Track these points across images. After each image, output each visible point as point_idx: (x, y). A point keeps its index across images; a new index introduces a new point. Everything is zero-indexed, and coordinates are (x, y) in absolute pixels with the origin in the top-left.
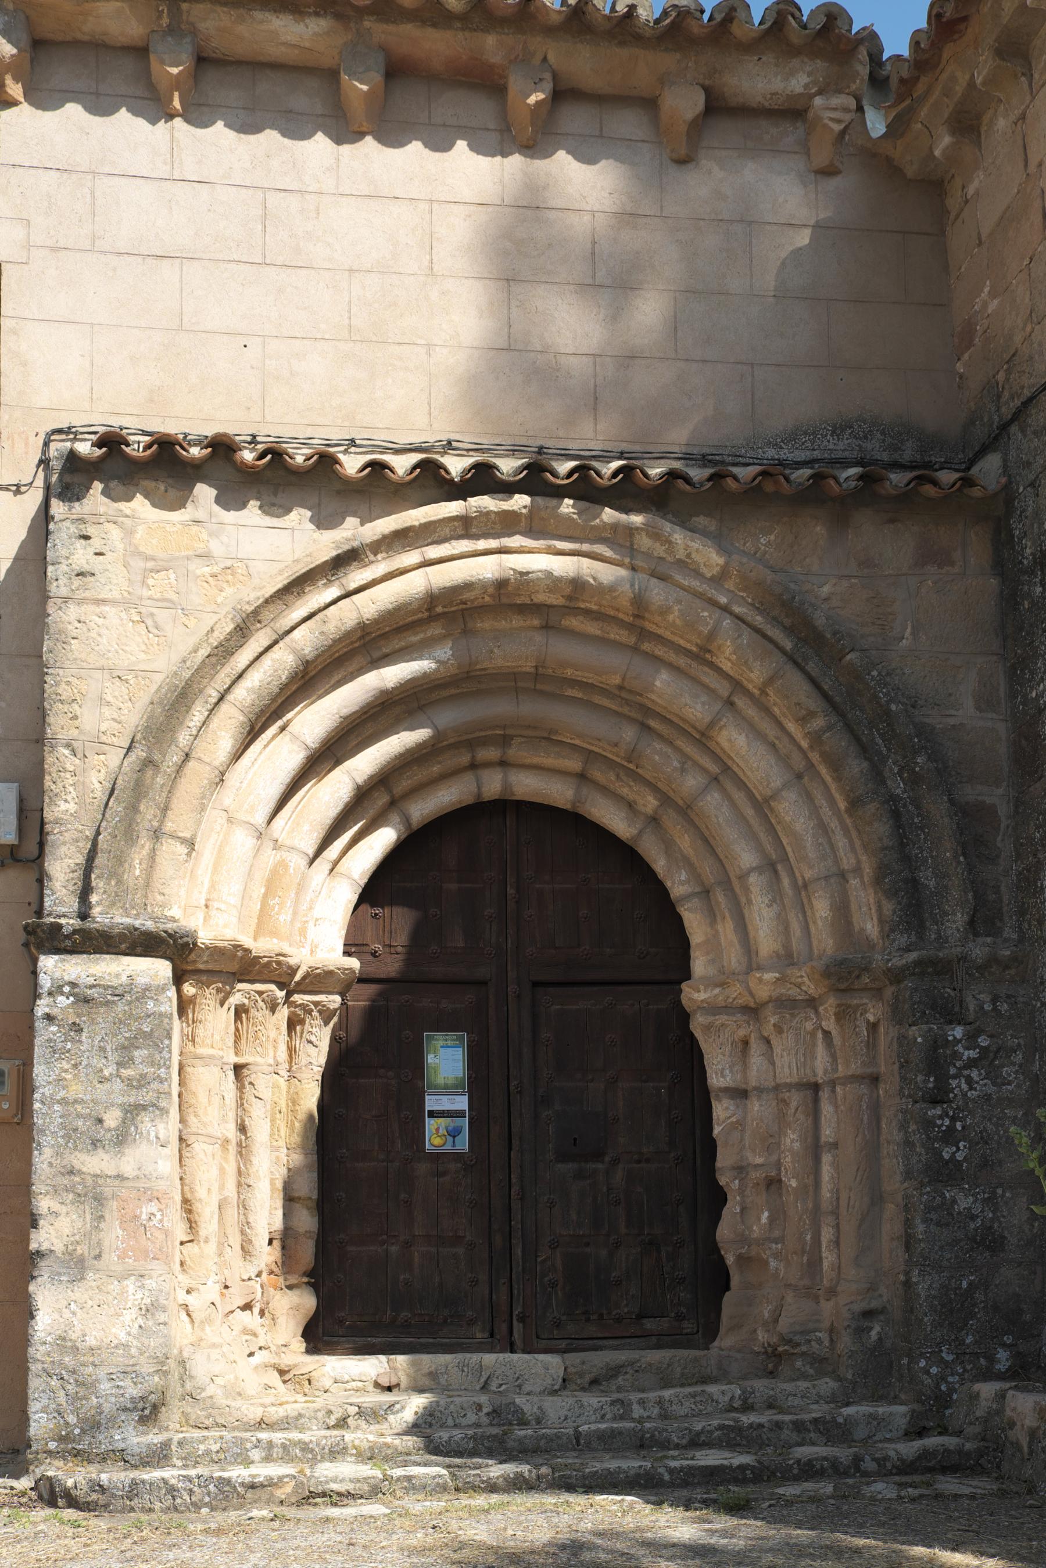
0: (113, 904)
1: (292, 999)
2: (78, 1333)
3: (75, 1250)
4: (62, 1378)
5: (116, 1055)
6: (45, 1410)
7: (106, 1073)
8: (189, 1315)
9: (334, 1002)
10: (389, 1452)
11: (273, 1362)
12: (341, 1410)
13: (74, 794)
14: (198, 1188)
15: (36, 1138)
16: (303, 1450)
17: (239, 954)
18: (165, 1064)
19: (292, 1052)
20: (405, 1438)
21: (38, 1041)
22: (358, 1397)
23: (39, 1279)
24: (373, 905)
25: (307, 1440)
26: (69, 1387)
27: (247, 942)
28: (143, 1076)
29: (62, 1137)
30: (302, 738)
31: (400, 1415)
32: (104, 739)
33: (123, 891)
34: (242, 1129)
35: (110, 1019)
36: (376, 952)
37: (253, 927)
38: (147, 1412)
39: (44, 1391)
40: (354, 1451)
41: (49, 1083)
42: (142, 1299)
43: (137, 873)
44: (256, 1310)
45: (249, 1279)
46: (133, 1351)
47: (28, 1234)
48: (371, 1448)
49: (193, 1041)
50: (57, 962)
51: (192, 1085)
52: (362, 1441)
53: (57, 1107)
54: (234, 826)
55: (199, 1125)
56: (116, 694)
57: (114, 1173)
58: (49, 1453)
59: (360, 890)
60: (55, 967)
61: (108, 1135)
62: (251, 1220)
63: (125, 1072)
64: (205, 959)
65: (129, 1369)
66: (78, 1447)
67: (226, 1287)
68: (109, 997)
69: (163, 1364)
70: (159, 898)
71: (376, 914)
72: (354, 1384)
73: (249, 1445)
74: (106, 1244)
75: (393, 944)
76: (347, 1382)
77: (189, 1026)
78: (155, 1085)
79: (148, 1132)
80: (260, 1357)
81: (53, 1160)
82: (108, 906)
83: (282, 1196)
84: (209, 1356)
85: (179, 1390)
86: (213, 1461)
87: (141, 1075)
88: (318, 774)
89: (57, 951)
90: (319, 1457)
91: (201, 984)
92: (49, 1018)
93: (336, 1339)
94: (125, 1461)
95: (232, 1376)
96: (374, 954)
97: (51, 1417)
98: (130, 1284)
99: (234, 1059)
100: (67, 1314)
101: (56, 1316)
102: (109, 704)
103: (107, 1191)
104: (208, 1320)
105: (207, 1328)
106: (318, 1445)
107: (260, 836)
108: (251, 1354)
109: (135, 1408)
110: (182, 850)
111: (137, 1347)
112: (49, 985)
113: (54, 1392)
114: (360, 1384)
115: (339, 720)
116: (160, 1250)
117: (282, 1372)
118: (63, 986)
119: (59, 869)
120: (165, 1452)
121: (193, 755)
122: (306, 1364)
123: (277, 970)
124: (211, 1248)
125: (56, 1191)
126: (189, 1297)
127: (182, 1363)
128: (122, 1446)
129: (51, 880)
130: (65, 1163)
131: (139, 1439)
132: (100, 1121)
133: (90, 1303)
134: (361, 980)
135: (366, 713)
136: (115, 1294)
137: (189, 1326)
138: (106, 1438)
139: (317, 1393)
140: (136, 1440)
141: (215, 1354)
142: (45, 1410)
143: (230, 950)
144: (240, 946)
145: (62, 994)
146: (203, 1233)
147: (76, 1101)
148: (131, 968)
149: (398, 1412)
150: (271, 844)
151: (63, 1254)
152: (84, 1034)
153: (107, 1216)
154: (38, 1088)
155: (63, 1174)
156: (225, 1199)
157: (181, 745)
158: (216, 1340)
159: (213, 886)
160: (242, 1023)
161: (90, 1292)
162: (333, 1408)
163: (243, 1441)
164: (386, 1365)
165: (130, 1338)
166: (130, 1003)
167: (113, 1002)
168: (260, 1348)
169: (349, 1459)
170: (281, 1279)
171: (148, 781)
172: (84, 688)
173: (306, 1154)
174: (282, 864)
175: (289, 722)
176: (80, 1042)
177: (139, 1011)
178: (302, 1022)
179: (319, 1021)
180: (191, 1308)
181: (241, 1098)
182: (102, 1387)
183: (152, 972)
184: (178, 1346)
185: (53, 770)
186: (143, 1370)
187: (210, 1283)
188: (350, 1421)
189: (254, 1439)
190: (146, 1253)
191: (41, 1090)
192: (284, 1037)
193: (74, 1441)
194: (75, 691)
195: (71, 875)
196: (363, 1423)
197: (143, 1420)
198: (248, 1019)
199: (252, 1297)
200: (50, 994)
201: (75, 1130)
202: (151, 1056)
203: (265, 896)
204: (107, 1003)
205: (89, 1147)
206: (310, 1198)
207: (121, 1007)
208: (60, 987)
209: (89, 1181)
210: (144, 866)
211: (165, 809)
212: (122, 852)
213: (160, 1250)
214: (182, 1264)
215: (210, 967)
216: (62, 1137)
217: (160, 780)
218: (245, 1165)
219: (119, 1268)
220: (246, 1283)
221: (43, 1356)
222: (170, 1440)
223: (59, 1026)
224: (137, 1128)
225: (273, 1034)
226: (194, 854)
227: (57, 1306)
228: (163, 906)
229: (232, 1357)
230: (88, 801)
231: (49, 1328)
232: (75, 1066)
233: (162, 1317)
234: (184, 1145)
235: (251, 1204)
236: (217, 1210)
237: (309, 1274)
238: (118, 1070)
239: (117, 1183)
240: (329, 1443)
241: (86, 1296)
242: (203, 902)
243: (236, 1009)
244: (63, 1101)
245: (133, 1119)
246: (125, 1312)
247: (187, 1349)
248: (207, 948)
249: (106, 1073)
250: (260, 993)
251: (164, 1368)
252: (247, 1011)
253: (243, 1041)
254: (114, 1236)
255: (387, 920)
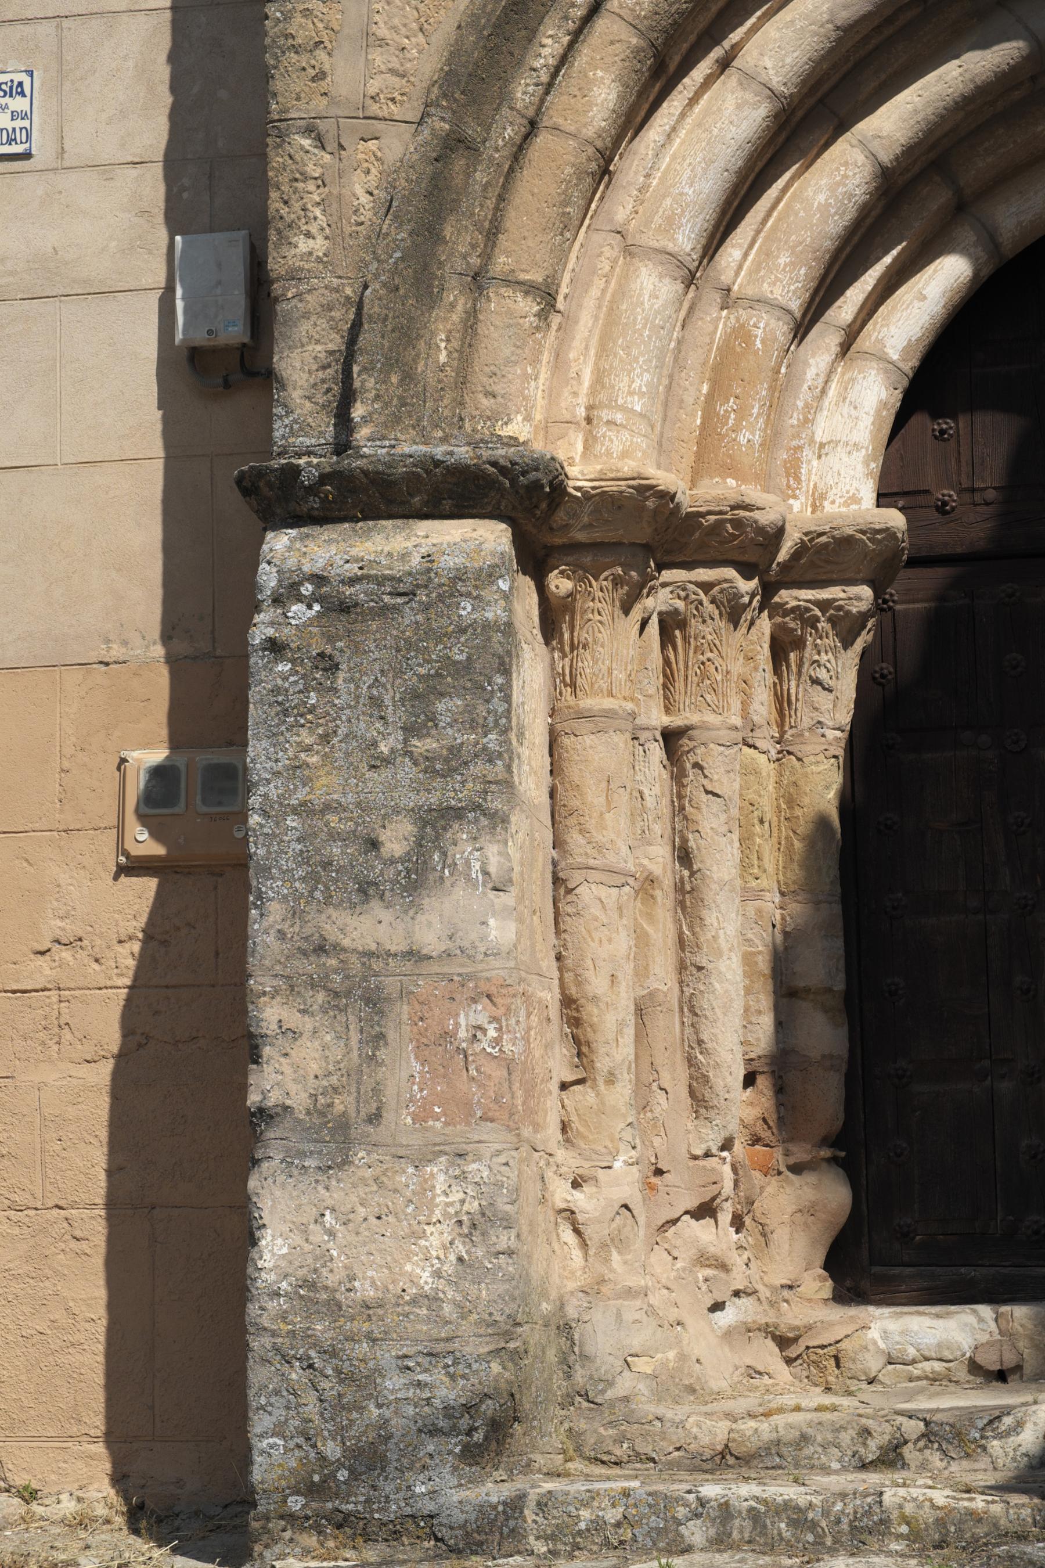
0: (396, 420)
1: (777, 599)
2: (340, 1274)
3: (331, 1105)
4: (311, 1366)
5: (401, 712)
6: (278, 1430)
7: (384, 748)
8: (577, 1231)
9: (859, 598)
10: (980, 1531)
11: (762, 1320)
12: (887, 1428)
13: (322, 220)
14: (590, 974)
15: (254, 883)
16: (793, 1523)
17: (650, 504)
18: (496, 722)
19: (782, 703)
20: (1016, 1499)
21: (253, 694)
22: (931, 1396)
23: (265, 1165)
24: (936, 415)
25: (802, 1501)
26: (325, 1384)
27: (665, 478)
28: (454, 750)
29: (303, 879)
30: (763, 78)
31: (1013, 1440)
32: (374, 109)
33: (416, 395)
34: (684, 856)
35: (390, 641)
36: (945, 504)
37: (689, 459)
38: (478, 1437)
39: (277, 1392)
40: (904, 1529)
41: (277, 774)
42: (463, 1202)
43: (443, 357)
44: (725, 1217)
45: (708, 1155)
46: (447, 1309)
47: (245, 1075)
48: (940, 1523)
49: (573, 685)
50: (292, 540)
51: (573, 772)
52: (920, 1507)
53: (291, 821)
54: (636, 261)
55: (589, 849)
56: (396, 21)
57: (403, 947)
58: (290, 1518)
59: (906, 383)
60: (289, 549)
61: (390, 873)
62: (705, 1037)
63: (421, 745)
64: (586, 519)
65: (439, 1347)
66: (343, 1507)
67: (659, 1172)
68: (387, 599)
69: (508, 1336)
70: (486, 402)
71: (942, 432)
72: (927, 1366)
73: (681, 1512)
74: (389, 1096)
75: (978, 485)
76: (914, 1362)
77: (564, 656)
78: (479, 768)
79: (468, 863)
80: (726, 1318)
81: (285, 927)
82: (385, 425)
83: (770, 987)
84: (619, 1315)
85: (559, 1385)
86: (607, 1544)
87: (451, 749)
88: (803, 154)
89: (297, 520)
90: (829, 1541)
91: (582, 572)
92: (275, 647)
93: (897, 1270)
94: (437, 1539)
95: (671, 1355)
96: (942, 509)
97: (291, 1444)
98: (438, 1173)
99: (658, 718)
100: (318, 1236)
101: (297, 1239)
102: (382, 42)
103: (391, 984)
104: (618, 1241)
105: (615, 1256)
106: (826, 1513)
107: (690, 280)
108: (717, 1307)
109: (454, 1427)
110: (528, 306)
111: (454, 1301)
112: (273, 584)
113: (295, 1395)
114: (938, 1366)
115: (833, 36)
116: (496, 1101)
117: (783, 1342)
118: (300, 583)
119: (298, 365)
120: (512, 1523)
121: (546, 121)
122: (828, 1325)
123: (734, 537)
124: (622, 1093)
125: (292, 987)
126: (577, 1195)
127: (566, 1329)
128: (429, 1507)
129: (283, 387)
130: (308, 930)
131: (463, 1494)
132: (374, 844)
133: (362, 1211)
134: (913, 562)
135: (889, 20)
136: (409, 1194)
137: (577, 1254)
138: (398, 1490)
139: (854, 1384)
140: (456, 1496)
141: (632, 1309)
142: (278, 1430)
143: (631, 497)
144: (651, 487)
145: (299, 598)
146: (602, 1064)
147: (327, 808)
148: (430, 541)
149: (1007, 1434)
150: (717, 297)
151: (308, 1113)
152: (341, 675)
153: (391, 1035)
154: (256, 785)
155: (304, 953)
156: (652, 995)
157: (519, 105)
158: (637, 1281)
159: (599, 380)
160: (675, 649)
161: (361, 1191)
162: (870, 1423)
163: (671, 1501)
164: (993, 1326)
165: (441, 1284)
166: (426, 607)
167: (395, 608)
168: (737, 1294)
169: (895, 1546)
170: (778, 1154)
171: (458, 180)
172: (335, 18)
173: (817, 903)
174: (741, 333)
175: (736, 48)
176: (336, 690)
177: (445, 621)
178: (799, 644)
179: (832, 640)
180: (580, 1217)
181: (680, 797)
182: (388, 1384)
183: (472, 545)
184: (554, 1295)
185: (284, 179)
186: (467, 1350)
187: (618, 1165)
188: (908, 1451)
189: (691, 1497)
190: (467, 1107)
191: (262, 790)
192: (763, 676)
193: (337, 1495)
194: (320, 25)
195: (321, 374)
196: (935, 1459)
197: (472, 1455)
198: (686, 639)
199: (713, 1190)
200: (277, 600)
201: (327, 865)
202: (469, 709)
203: (710, 397)
204: (384, 611)
205: (355, 899)
206: (829, 990)
207: (409, 617)
208: (295, 586)
209: (355, 964)
210: (455, 344)
211: (493, 232)
212: (411, 319)
213: (496, 1101)
214: (564, 1127)
215: (597, 536)
216: (303, 879)
217: (480, 176)
218: (691, 928)
219: (415, 1140)
220: (701, 1163)
221: (274, 1320)
222: (522, 1497)
223: (293, 661)
224: (445, 854)
225: (737, 667)
226: (556, 320)
227: (299, 1220)
228: (492, 418)
229: (674, 1314)
230: (348, 230)
231: (283, 1263)
232: (325, 738)
233: (504, 1239)
234: (562, 891)
235: (703, 1003)
236: (631, 1019)
237: (835, 1141)
238: (406, 741)
239: (408, 966)
240: (849, 1510)
241: (353, 1198)
242: (581, 412)
243: (661, 622)
244: (303, 809)
245: (437, 838)
246: (429, 1229)
247: (574, 1302)
248: (587, 496)
249: (384, 748)
250: (706, 587)
251: (512, 1345)
252: (683, 625)
253: (680, 684)
254: (405, 1075)
255: (965, 449)
